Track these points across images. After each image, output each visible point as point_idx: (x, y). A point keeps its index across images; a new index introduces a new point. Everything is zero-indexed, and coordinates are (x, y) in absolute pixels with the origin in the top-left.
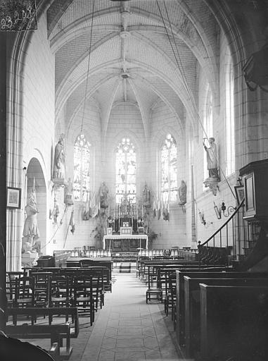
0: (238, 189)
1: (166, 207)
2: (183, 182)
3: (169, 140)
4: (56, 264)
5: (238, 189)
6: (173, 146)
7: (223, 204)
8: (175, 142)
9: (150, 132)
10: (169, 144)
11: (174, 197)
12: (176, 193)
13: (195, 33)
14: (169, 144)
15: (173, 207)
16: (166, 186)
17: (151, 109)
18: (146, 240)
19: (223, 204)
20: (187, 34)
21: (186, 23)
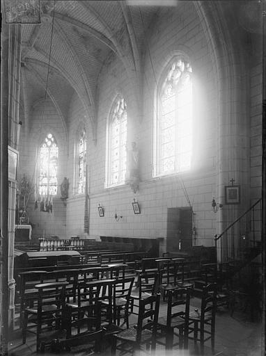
0: (228, 189)
1: (49, 199)
2: (65, 179)
3: (50, 139)
4: (161, 254)
5: (228, 189)
6: (54, 145)
7: (214, 201)
8: (55, 142)
9: (30, 128)
10: (49, 143)
11: (54, 191)
12: (56, 188)
13: (128, 45)
14: (49, 143)
15: (55, 200)
16: (45, 181)
17: (32, 106)
18: (29, 230)
19: (214, 201)
20: (121, 42)
21: (122, 31)
